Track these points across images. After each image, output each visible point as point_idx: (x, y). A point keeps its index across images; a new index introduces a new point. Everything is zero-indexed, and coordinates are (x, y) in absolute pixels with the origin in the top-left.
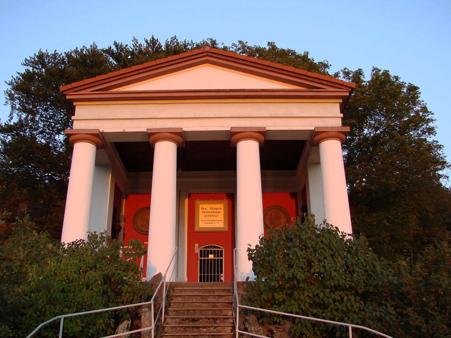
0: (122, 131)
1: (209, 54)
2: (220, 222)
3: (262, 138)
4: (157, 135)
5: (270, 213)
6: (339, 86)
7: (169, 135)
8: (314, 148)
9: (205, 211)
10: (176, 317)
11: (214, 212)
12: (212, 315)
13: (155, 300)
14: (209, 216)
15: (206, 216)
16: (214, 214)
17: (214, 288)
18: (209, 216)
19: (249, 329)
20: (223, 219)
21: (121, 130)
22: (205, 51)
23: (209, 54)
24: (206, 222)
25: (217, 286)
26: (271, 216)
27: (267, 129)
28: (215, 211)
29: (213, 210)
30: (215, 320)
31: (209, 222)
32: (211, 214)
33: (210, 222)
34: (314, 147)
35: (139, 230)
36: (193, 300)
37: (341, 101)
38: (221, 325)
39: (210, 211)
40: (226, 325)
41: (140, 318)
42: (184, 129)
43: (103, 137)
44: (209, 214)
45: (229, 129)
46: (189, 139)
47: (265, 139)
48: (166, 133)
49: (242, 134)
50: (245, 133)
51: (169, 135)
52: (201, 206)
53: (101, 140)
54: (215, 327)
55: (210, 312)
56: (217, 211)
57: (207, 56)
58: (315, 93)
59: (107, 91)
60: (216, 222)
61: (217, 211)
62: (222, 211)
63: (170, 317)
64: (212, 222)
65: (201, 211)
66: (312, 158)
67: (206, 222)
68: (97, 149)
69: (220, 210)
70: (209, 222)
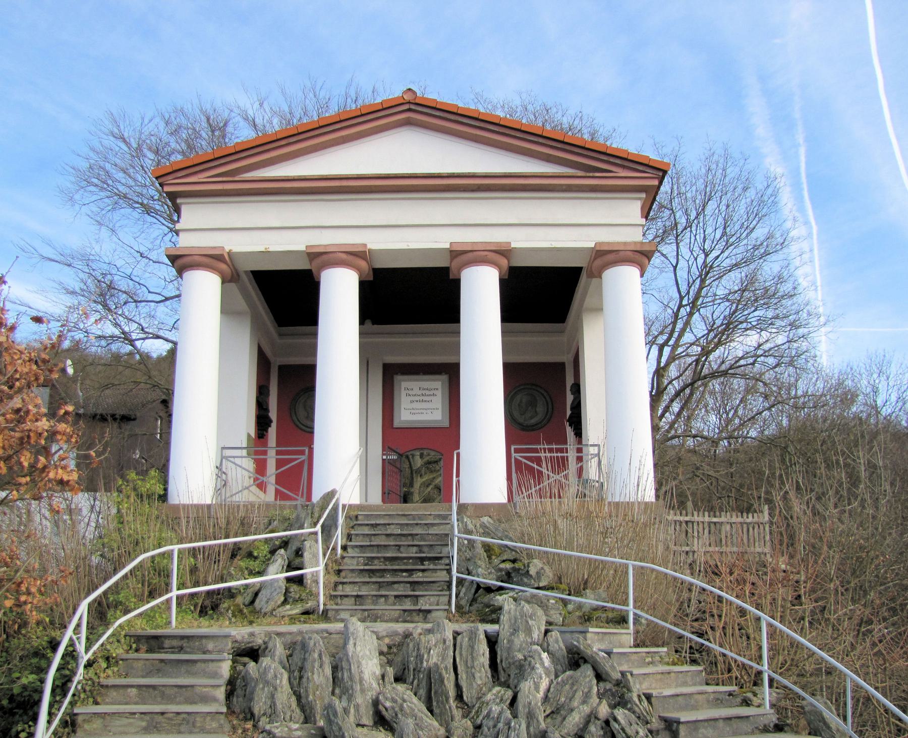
0: (263, 250)
1: (413, 107)
2: (435, 412)
3: (504, 263)
4: (325, 257)
5: (518, 397)
6: (641, 168)
7: (344, 256)
8: (595, 280)
9: (411, 392)
10: (359, 555)
11: (425, 395)
12: (416, 553)
13: (323, 526)
14: (417, 401)
15: (412, 402)
16: (425, 398)
17: (421, 513)
18: (417, 401)
19: (474, 572)
20: (439, 406)
21: (261, 248)
22: (404, 102)
23: (413, 107)
24: (413, 411)
25: (425, 509)
26: (521, 402)
27: (513, 246)
28: (427, 392)
29: (424, 392)
30: (422, 560)
31: (417, 411)
32: (421, 398)
33: (420, 411)
34: (594, 280)
35: (303, 425)
36: (386, 530)
37: (643, 195)
38: (432, 567)
39: (420, 392)
40: (439, 567)
41: (302, 556)
42: (370, 246)
43: (233, 265)
44: (417, 398)
45: (447, 246)
46: (380, 264)
47: (511, 265)
48: (340, 254)
49: (470, 255)
50: (475, 253)
51: (344, 256)
52: (404, 385)
53: (228, 266)
54: (423, 571)
55: (415, 549)
56: (431, 393)
57: (409, 110)
58: (598, 179)
59: (234, 176)
60: (429, 411)
61: (431, 393)
62: (439, 393)
63: (349, 555)
64: (422, 411)
65: (403, 393)
66: (589, 301)
67: (413, 411)
68: (223, 283)
69: (435, 392)
70: (417, 411)
